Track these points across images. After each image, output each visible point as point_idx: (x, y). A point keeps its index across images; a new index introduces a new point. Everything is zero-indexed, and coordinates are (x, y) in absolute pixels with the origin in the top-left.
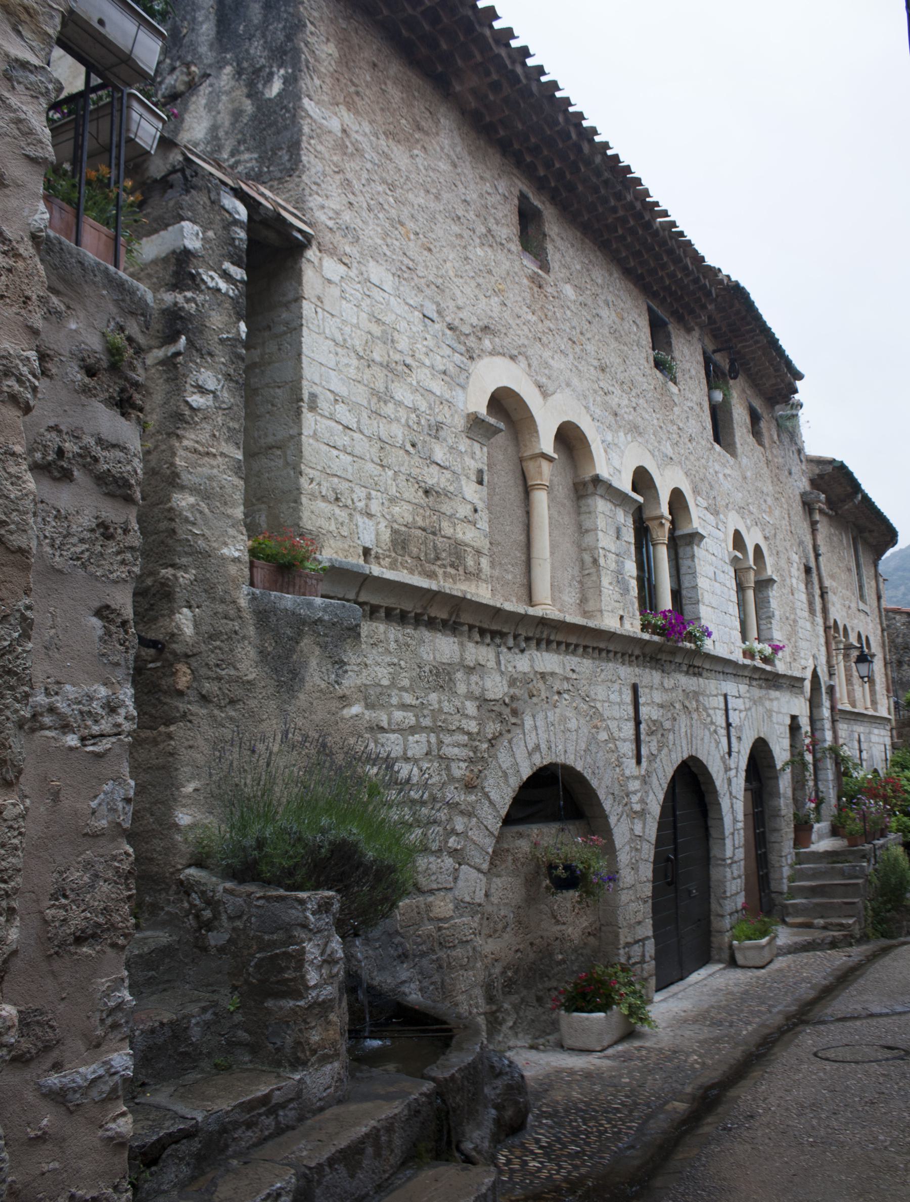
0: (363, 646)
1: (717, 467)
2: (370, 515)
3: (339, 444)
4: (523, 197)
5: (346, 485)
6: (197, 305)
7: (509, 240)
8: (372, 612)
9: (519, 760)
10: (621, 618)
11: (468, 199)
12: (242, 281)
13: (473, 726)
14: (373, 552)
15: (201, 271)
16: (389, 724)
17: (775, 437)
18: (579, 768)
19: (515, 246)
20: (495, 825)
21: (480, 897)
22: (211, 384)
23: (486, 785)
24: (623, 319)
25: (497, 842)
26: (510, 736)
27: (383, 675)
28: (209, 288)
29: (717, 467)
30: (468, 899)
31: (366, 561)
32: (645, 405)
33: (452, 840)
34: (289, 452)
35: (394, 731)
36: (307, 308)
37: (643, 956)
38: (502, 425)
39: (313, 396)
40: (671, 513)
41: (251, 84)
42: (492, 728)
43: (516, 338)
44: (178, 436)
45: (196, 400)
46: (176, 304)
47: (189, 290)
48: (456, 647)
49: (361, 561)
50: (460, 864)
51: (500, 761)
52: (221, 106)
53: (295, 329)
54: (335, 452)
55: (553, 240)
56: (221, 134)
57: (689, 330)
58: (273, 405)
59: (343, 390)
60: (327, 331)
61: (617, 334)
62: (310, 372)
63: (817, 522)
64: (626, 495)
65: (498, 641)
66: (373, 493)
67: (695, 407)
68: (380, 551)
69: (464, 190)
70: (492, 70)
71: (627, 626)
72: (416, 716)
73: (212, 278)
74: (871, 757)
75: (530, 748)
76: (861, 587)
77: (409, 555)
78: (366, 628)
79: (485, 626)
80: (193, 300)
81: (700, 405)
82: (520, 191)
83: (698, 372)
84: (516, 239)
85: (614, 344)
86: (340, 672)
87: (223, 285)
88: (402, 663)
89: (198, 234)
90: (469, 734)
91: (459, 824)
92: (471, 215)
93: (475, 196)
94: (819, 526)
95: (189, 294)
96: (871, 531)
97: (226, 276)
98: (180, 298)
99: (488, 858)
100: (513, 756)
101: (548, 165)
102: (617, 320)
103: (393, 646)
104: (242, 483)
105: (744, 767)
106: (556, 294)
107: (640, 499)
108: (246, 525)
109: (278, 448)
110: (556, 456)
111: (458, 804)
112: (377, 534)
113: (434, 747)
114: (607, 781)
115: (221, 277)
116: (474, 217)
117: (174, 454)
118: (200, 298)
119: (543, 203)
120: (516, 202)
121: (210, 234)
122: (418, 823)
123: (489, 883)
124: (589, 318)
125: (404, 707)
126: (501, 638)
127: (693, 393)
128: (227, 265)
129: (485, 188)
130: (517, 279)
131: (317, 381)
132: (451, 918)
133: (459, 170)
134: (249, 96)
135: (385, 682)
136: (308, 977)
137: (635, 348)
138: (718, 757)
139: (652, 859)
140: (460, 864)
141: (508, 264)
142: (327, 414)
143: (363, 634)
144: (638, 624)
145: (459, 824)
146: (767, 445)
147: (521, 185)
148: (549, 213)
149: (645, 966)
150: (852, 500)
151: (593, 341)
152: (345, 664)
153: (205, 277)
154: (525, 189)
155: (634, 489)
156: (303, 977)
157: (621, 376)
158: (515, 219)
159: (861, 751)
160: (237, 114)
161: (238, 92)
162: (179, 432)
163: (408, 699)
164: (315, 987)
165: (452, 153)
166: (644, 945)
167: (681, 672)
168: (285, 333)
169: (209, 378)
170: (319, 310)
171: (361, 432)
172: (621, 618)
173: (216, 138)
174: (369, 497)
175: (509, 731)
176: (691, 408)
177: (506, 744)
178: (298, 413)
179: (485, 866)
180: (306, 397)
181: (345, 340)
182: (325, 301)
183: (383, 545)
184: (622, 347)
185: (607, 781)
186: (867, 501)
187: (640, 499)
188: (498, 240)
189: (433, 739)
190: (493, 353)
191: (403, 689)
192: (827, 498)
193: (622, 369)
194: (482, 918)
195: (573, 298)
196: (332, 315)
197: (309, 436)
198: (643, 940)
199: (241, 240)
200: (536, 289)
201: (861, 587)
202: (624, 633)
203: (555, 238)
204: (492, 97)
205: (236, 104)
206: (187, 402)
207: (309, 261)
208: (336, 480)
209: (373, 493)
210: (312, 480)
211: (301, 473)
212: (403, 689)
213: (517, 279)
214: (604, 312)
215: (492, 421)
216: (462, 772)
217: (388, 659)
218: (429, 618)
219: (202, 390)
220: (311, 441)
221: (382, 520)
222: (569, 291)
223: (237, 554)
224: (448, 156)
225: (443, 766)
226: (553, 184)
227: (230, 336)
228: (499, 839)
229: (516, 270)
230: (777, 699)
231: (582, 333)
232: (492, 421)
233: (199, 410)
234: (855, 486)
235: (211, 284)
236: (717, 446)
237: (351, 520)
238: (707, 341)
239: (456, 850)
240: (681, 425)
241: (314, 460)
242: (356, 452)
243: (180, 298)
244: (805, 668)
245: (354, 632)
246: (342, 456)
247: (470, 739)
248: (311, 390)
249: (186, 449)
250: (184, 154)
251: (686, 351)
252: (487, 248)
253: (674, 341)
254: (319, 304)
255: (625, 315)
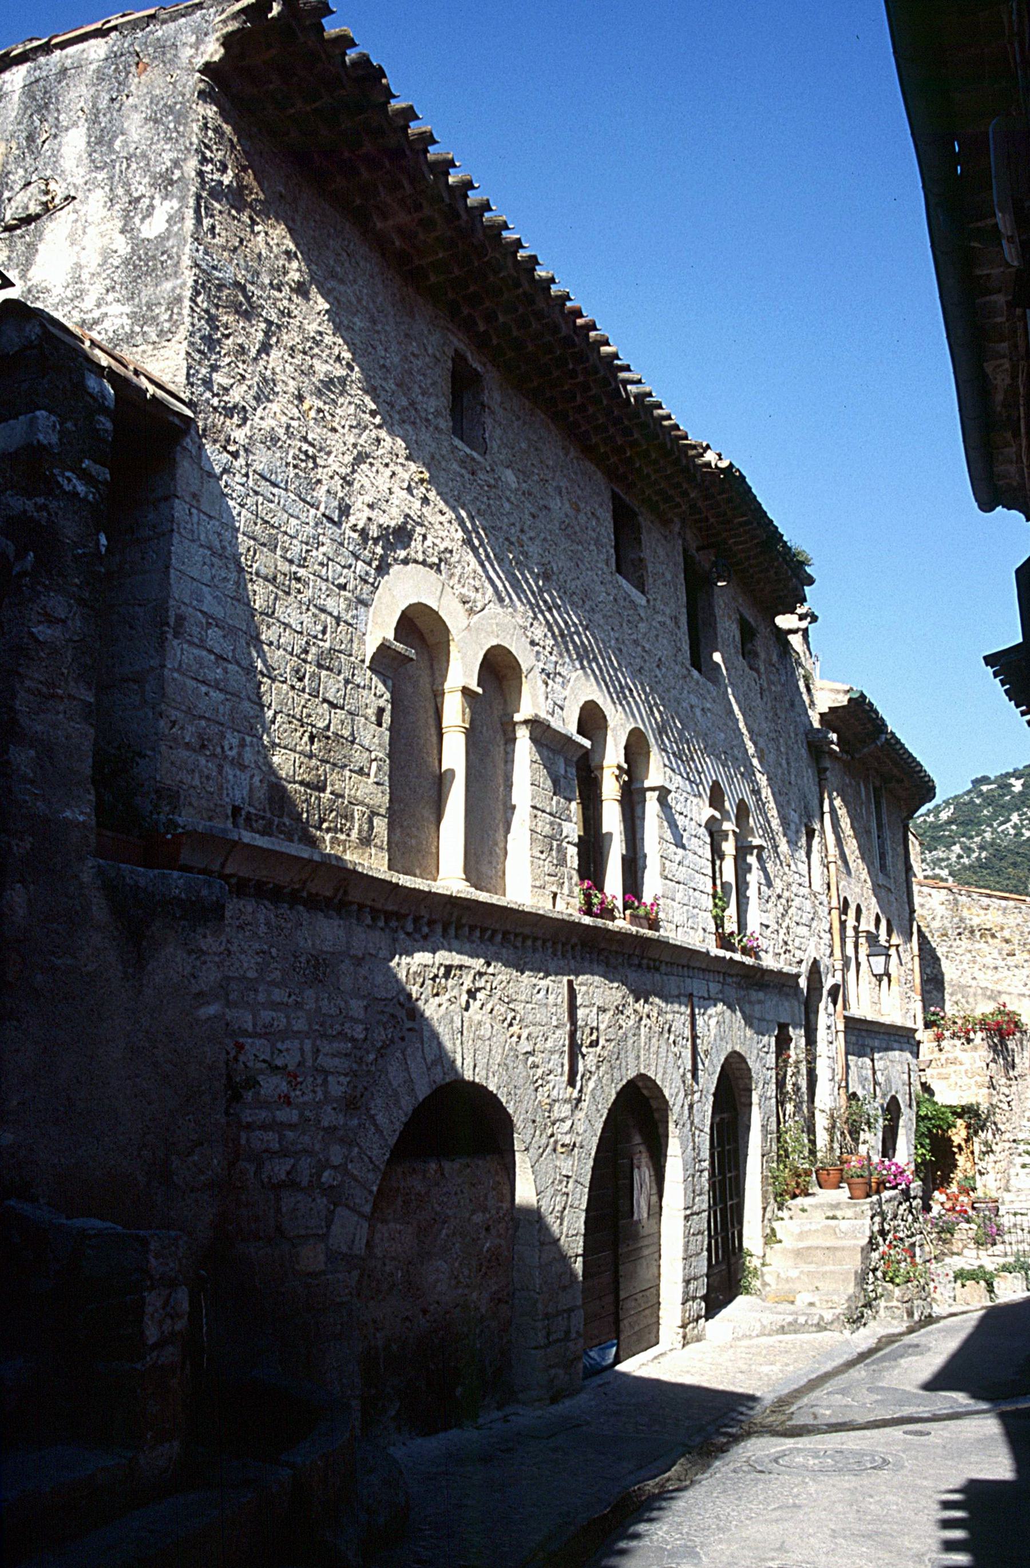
0: (228, 929)
1: (694, 700)
2: (243, 768)
3: (211, 676)
4: (459, 358)
5: (216, 729)
6: (49, 514)
7: (437, 414)
8: (241, 888)
9: (414, 1076)
10: (555, 895)
11: (388, 363)
12: (105, 483)
13: (359, 1033)
14: (243, 813)
15: (56, 471)
16: (255, 1025)
17: (775, 658)
18: (492, 1088)
19: (445, 424)
20: (380, 1154)
21: (360, 1247)
22: (61, 613)
23: (372, 1105)
24: (578, 510)
25: (383, 1179)
26: (403, 1045)
27: (248, 965)
28: (66, 493)
29: (694, 700)
30: (344, 1249)
31: (235, 824)
32: (602, 622)
33: (326, 1174)
34: (148, 687)
35: (260, 1036)
36: (180, 509)
37: (567, 1332)
38: (412, 653)
39: (181, 619)
40: (626, 761)
41: (127, 217)
42: (380, 1035)
43: (438, 541)
44: (19, 674)
45: (43, 631)
46: (25, 511)
47: (40, 496)
48: (341, 933)
49: (229, 825)
50: (335, 1205)
51: (391, 1076)
52: (86, 241)
53: (165, 533)
54: (204, 689)
55: (493, 412)
56: (85, 277)
57: (666, 522)
58: (131, 627)
59: (218, 612)
60: (202, 537)
61: (569, 531)
62: (180, 590)
63: (826, 769)
64: (569, 739)
65: (393, 924)
66: (248, 739)
67: (668, 622)
68: (253, 811)
69: (383, 353)
70: (425, 204)
71: (561, 905)
72: (287, 1017)
73: (69, 480)
74: (888, 1080)
75: (429, 1061)
76: (882, 856)
77: (289, 816)
78: (232, 907)
79: (378, 905)
80: (44, 507)
81: (675, 619)
82: (456, 350)
83: (675, 576)
84: (446, 413)
85: (565, 544)
86: (198, 963)
87: (81, 489)
88: (274, 951)
89: (54, 426)
90: (353, 1040)
91: (336, 1154)
92: (391, 385)
93: (396, 360)
94: (828, 773)
95: (41, 500)
96: (900, 781)
97: (85, 476)
98: (29, 505)
99: (371, 1199)
100: (407, 1070)
101: (490, 318)
102: (571, 513)
103: (263, 928)
104: (92, 731)
105: (712, 1090)
106: (492, 482)
107: (587, 743)
108: (93, 782)
109: (135, 681)
110: (480, 690)
111: (335, 1128)
112: (251, 790)
113: (309, 1055)
114: (528, 1104)
115: (79, 478)
116: (393, 386)
117: (14, 697)
118: (53, 505)
119: (484, 365)
120: (450, 364)
121: (69, 425)
122: (284, 1153)
123: (372, 1229)
124: (533, 510)
125: (275, 1006)
126: (397, 920)
127: (666, 604)
128: (86, 463)
129: (410, 349)
130: (443, 464)
131: (187, 601)
132: (323, 1273)
133: (379, 327)
134: (122, 232)
135: (251, 974)
136: (148, 1333)
137: (592, 547)
138: (677, 1076)
139: (584, 1206)
140: (335, 1205)
141: (434, 445)
142: (196, 641)
143: (228, 914)
144: (578, 901)
145: (336, 1154)
146: (762, 669)
147: (458, 342)
148: (491, 377)
149: (571, 1344)
150: (874, 741)
151: (537, 542)
152: (204, 953)
153: (60, 479)
154: (461, 347)
155: (579, 732)
156: (142, 1333)
157: (572, 586)
158: (446, 386)
159: (874, 1073)
160: (107, 254)
161: (109, 225)
162: (21, 670)
163: (279, 995)
164: (156, 1346)
165: (371, 305)
166: (569, 1317)
167: (630, 965)
168: (150, 539)
169: (58, 605)
170: (194, 511)
171: (239, 664)
172: (555, 895)
173: (78, 280)
174: (242, 744)
175: (403, 1039)
176: (663, 624)
177: (398, 1054)
178: (162, 640)
179: (367, 1209)
180: (172, 621)
181: (224, 548)
182: (203, 500)
183: (257, 804)
184: (575, 547)
185: (528, 1104)
186: (894, 745)
187: (587, 743)
188: (423, 415)
189: (308, 1045)
190: (405, 562)
191: (273, 983)
192: (838, 738)
193: (574, 575)
194: (361, 1276)
195: (514, 486)
196: (210, 517)
197: (173, 670)
198: (571, 1310)
199: (106, 431)
200: (467, 476)
201: (882, 856)
202: (555, 915)
203: (496, 408)
204: (422, 237)
205: (106, 241)
206: (32, 634)
207: (185, 449)
208: (203, 723)
209: (248, 739)
210: (174, 723)
211: (161, 715)
212: (273, 983)
213: (443, 464)
214: (555, 504)
215: (400, 647)
216: (343, 1089)
217: (256, 946)
218: (310, 894)
219: (51, 620)
220: (176, 675)
221: (256, 772)
222: (510, 477)
223: (81, 818)
224: (367, 309)
225: (319, 1081)
226: (495, 342)
227: (87, 550)
228: (386, 1176)
229: (444, 452)
230: (760, 1002)
231: (522, 531)
232: (400, 647)
233: (45, 643)
234: (879, 725)
235: (68, 488)
236: (695, 673)
237: (220, 773)
238: (689, 536)
239: (331, 1187)
240: (647, 646)
241: (179, 699)
242: (230, 689)
243: (29, 505)
244: (800, 962)
245: (217, 911)
246: (215, 694)
247: (355, 1047)
248: (179, 612)
249: (29, 690)
250: (43, 326)
251: (661, 552)
252: (407, 427)
253: (644, 537)
254: (194, 503)
255: (582, 505)
